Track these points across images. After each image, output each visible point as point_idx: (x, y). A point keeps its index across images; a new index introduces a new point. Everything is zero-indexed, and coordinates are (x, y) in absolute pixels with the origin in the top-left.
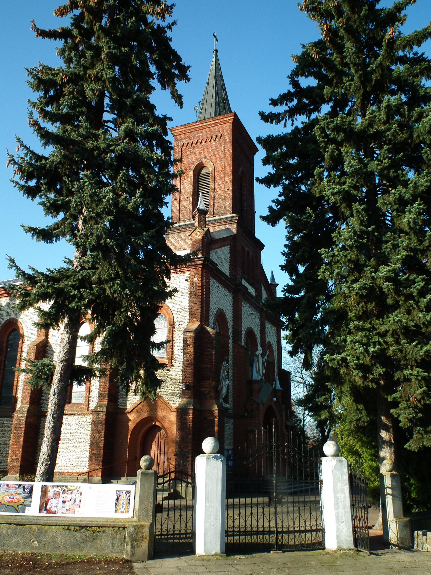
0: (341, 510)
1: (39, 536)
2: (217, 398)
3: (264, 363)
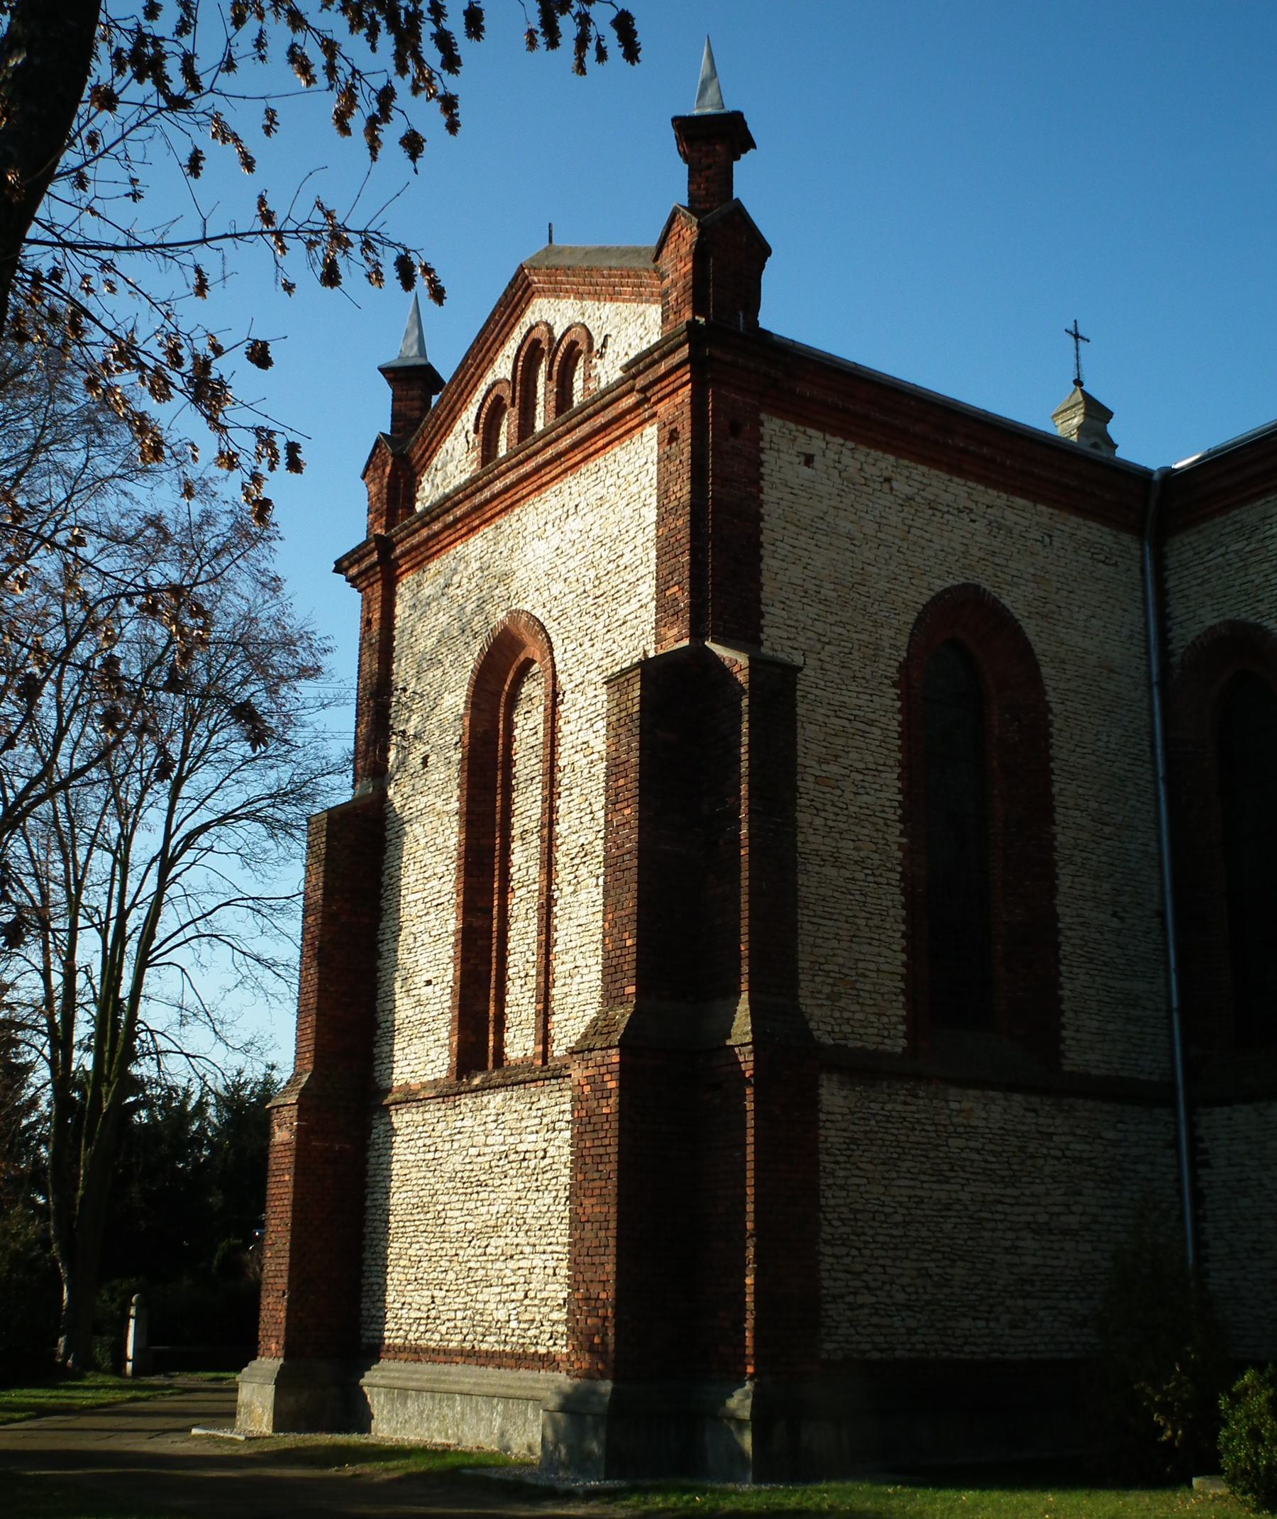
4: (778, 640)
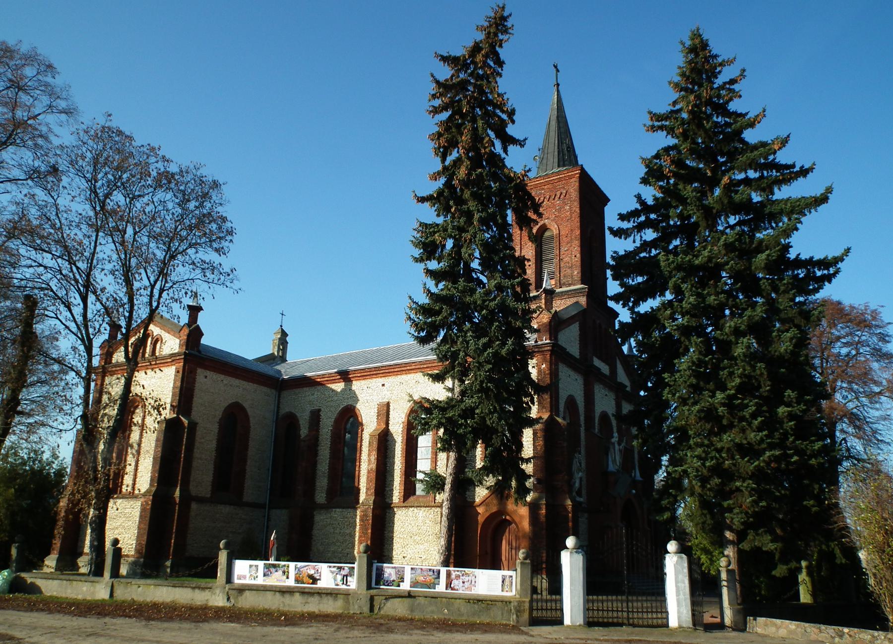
0: (682, 597)
1: (448, 605)
2: (570, 492)
3: (620, 451)
4: (195, 415)
